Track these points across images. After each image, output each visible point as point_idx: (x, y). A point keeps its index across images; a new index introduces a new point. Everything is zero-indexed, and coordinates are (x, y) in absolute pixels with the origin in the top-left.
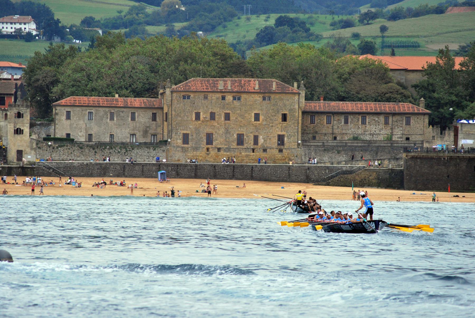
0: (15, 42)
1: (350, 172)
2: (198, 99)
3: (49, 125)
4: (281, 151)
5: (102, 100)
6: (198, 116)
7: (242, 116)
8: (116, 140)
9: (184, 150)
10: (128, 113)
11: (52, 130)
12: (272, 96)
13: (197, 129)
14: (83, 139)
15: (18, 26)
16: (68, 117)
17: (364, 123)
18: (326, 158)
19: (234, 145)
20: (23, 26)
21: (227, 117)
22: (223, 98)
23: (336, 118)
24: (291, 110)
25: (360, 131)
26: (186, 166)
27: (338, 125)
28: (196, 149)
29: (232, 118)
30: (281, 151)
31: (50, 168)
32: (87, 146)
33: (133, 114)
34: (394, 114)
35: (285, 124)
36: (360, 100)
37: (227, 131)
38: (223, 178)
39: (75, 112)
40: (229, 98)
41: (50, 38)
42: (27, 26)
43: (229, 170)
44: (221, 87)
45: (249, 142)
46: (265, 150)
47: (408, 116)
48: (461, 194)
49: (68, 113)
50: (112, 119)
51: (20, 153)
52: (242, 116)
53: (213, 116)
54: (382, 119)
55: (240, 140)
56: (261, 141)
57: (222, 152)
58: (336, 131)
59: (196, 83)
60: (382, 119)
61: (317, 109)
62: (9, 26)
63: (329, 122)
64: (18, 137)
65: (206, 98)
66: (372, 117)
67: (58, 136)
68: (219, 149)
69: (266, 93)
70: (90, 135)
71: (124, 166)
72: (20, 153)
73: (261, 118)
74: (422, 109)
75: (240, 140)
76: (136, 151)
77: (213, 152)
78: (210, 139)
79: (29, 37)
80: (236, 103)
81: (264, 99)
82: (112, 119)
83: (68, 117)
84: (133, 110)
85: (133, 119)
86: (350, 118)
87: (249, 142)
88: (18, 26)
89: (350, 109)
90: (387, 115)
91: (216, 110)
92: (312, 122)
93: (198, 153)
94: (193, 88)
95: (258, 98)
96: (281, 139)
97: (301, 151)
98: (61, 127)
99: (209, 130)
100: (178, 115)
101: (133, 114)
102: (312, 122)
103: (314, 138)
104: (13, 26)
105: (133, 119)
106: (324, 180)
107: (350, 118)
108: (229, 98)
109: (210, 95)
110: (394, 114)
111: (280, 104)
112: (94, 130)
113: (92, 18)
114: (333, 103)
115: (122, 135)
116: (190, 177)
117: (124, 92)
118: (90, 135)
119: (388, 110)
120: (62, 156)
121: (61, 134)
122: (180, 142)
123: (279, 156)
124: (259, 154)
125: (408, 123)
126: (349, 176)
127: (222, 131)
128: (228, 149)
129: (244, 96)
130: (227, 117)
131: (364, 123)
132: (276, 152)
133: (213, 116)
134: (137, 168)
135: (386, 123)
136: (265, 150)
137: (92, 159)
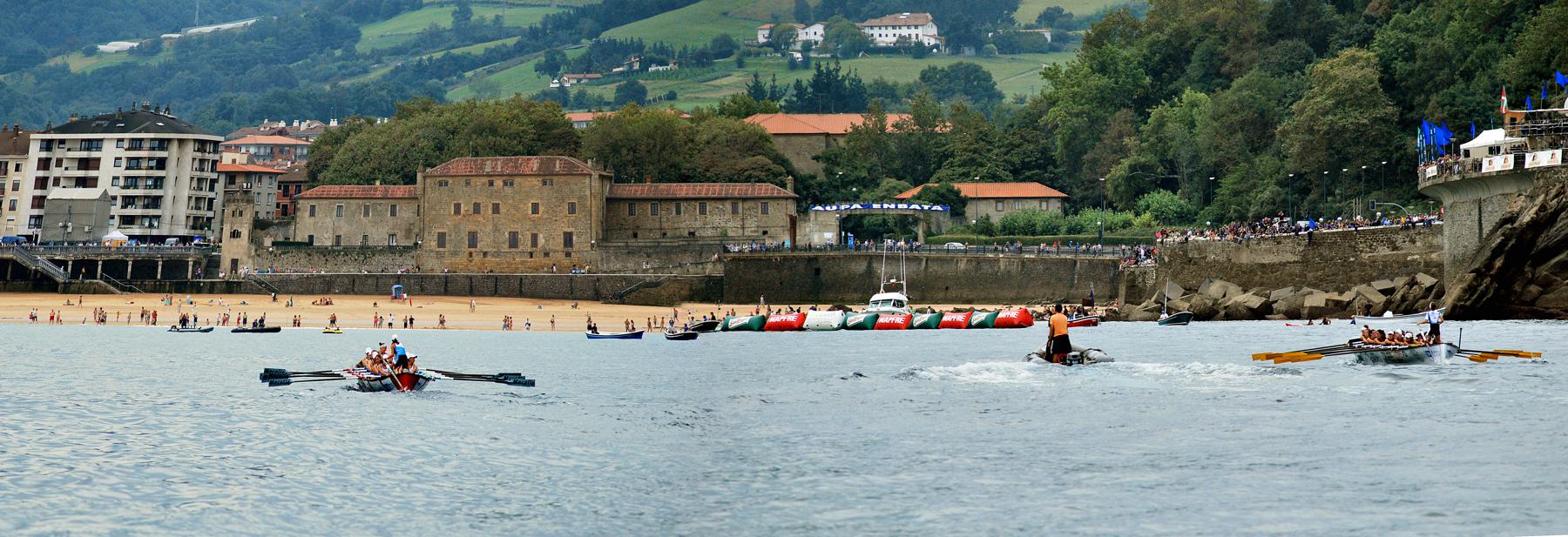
0: (895, 60)
1: (656, 284)
2: (458, 186)
3: (289, 224)
4: (568, 255)
5: (355, 189)
6: (458, 207)
7: (517, 208)
8: (370, 243)
9: (440, 256)
10: (387, 204)
11: (291, 232)
12: (555, 179)
13: (455, 226)
14: (329, 243)
15: (905, 32)
16: (312, 214)
17: (703, 212)
18: (631, 265)
19: (505, 248)
20: (913, 31)
21: (496, 209)
22: (491, 184)
23: (665, 206)
24: (580, 198)
25: (698, 224)
26: (433, 277)
27: (667, 216)
28: (455, 254)
29: (503, 210)
30: (568, 255)
31: (261, 283)
32: (908, 259)
33: (393, 207)
34: (745, 200)
35: (573, 217)
36: (709, 180)
37: (496, 229)
38: (483, 295)
39: (321, 206)
40: (499, 183)
41: (957, 51)
42: (920, 31)
43: (491, 284)
44: (488, 169)
45: (525, 244)
46: (547, 254)
47: (764, 201)
48: (780, 313)
49: (313, 207)
50: (367, 214)
51: (235, 262)
52: (517, 208)
53: (477, 208)
54: (728, 205)
55: (514, 241)
56: (541, 241)
57: (489, 258)
58: (665, 225)
59: (459, 165)
60: (728, 205)
61: (638, 195)
62: (890, 31)
63: (654, 213)
64: (235, 241)
65: (468, 184)
66: (714, 204)
67: (299, 239)
68: (485, 254)
69: (546, 175)
70: (339, 237)
71: (353, 279)
72: (235, 262)
73: (541, 209)
74: (790, 192)
75: (514, 241)
76: (377, 257)
77: (477, 258)
78: (473, 240)
79: (920, 51)
80: (508, 190)
81: (545, 183)
82: (367, 214)
83: (312, 214)
84: (393, 202)
85: (393, 214)
86: (683, 206)
87: (525, 244)
88: (905, 32)
89: (683, 194)
90: (735, 200)
91: (481, 200)
92: (631, 213)
93: (457, 260)
94: (452, 172)
95: (537, 182)
96: (568, 239)
97: (595, 255)
98: (303, 228)
99: (471, 228)
100: (432, 208)
101: (393, 207)
102: (631, 213)
103: (635, 236)
104: (898, 32)
105: (393, 214)
106: (621, 297)
107: (683, 206)
108: (499, 183)
109: (473, 180)
110: (745, 200)
111: (566, 190)
112: (344, 230)
113: (1059, 10)
114: (663, 186)
115: (378, 237)
116: (438, 294)
117: (393, 177)
118: (339, 237)
119: (736, 194)
120: (291, 266)
121: (301, 237)
122: (434, 244)
123: (566, 262)
124: (539, 259)
125: (765, 211)
126: (653, 291)
127: (490, 227)
128: (497, 254)
129: (517, 180)
130: (496, 209)
131: (703, 212)
132: (561, 256)
133: (477, 208)
134: (370, 281)
135: (735, 212)
136: (547, 254)
137: (349, 269)
